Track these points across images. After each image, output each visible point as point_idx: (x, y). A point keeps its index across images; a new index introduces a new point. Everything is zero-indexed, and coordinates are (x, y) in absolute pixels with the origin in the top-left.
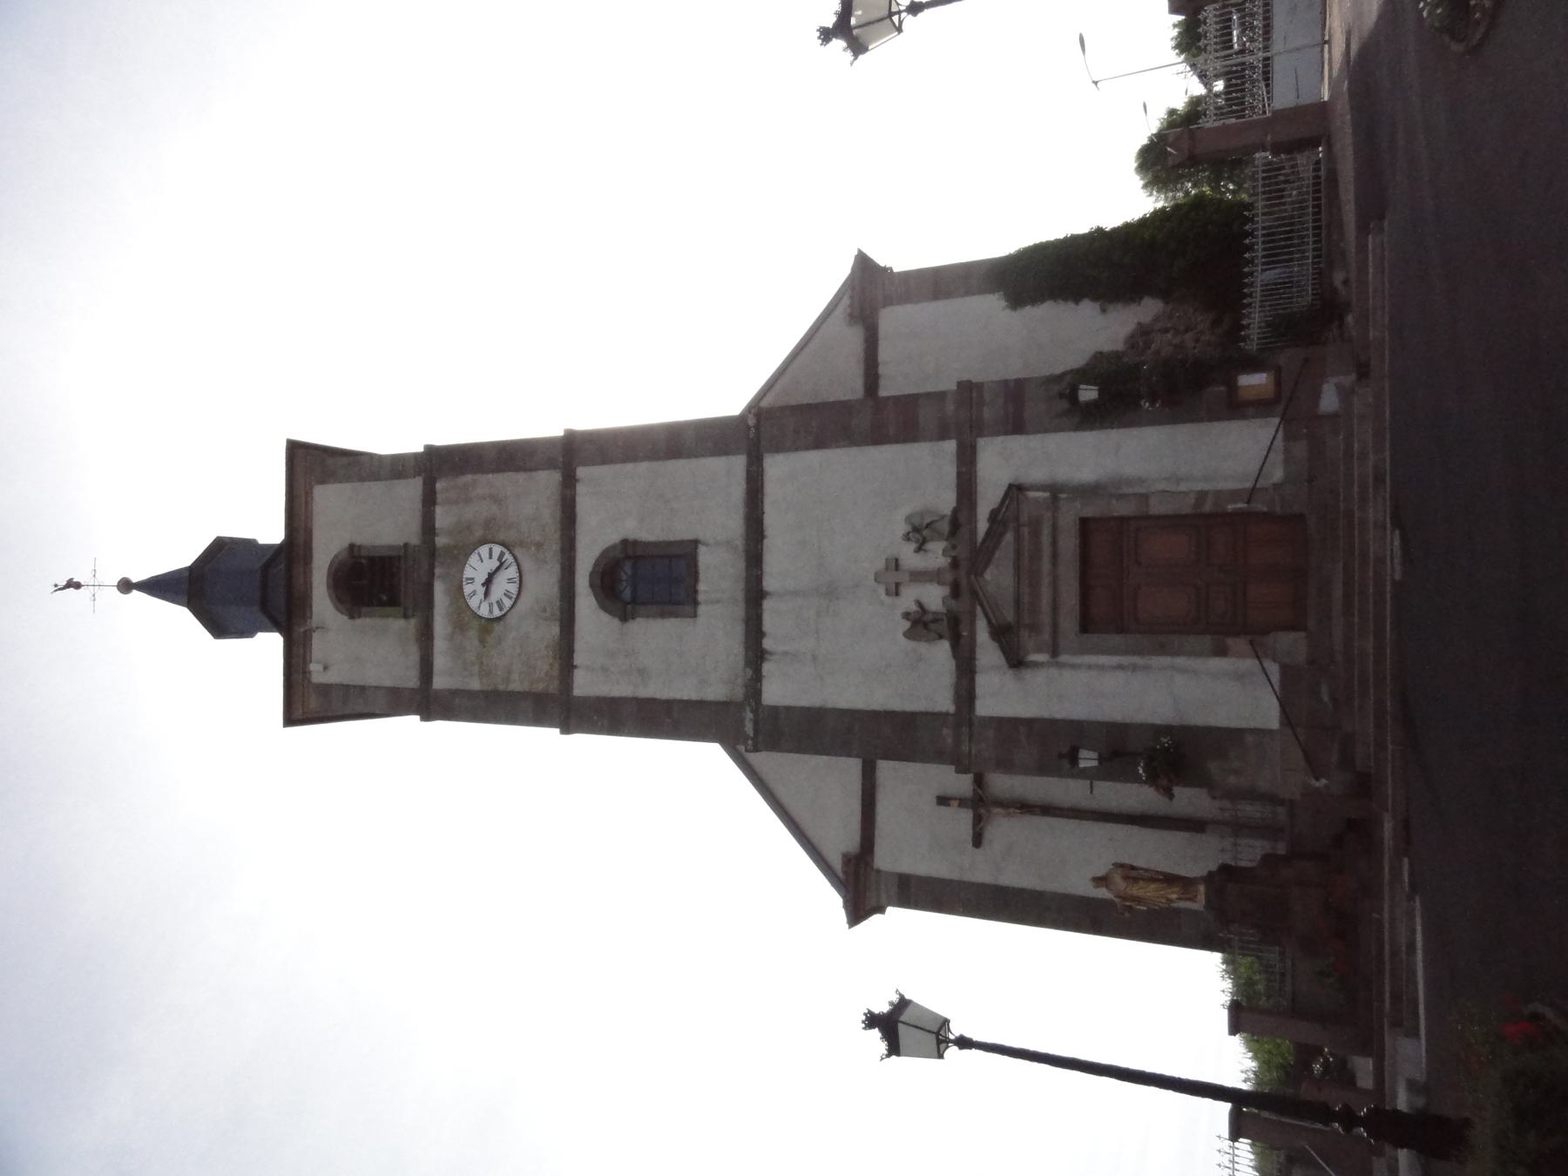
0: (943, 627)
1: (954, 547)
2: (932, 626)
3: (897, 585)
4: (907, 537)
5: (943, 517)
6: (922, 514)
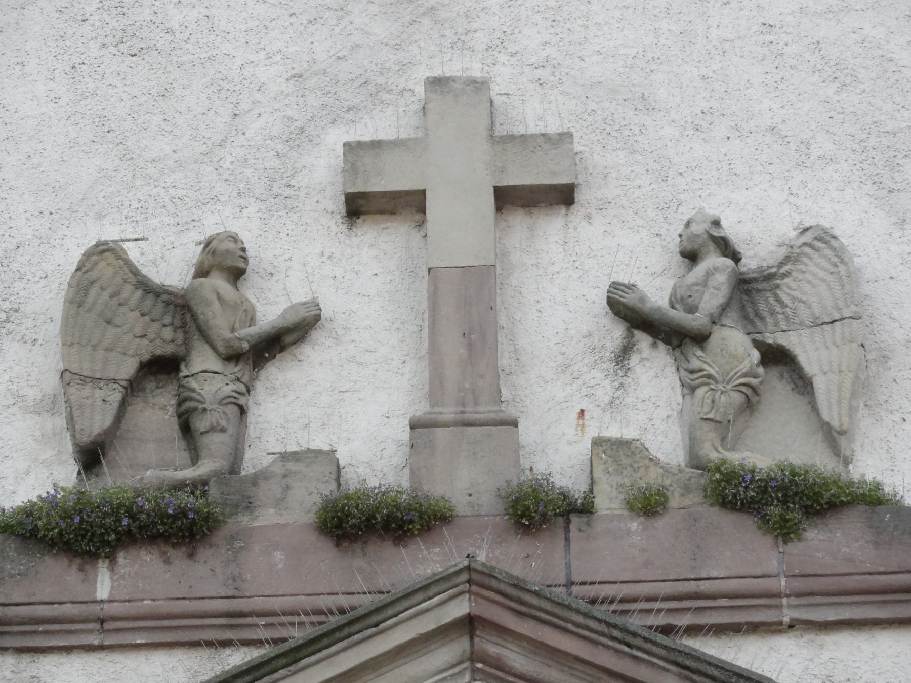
0: (151, 464)
1: (649, 505)
2: (156, 413)
3: (410, 204)
4: (705, 244)
5: (833, 437)
6: (848, 315)
